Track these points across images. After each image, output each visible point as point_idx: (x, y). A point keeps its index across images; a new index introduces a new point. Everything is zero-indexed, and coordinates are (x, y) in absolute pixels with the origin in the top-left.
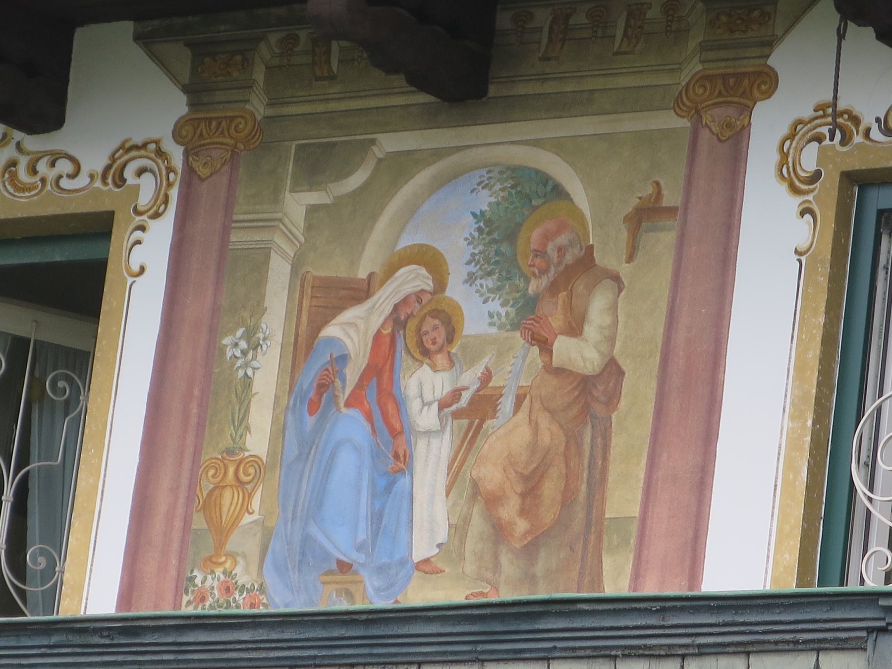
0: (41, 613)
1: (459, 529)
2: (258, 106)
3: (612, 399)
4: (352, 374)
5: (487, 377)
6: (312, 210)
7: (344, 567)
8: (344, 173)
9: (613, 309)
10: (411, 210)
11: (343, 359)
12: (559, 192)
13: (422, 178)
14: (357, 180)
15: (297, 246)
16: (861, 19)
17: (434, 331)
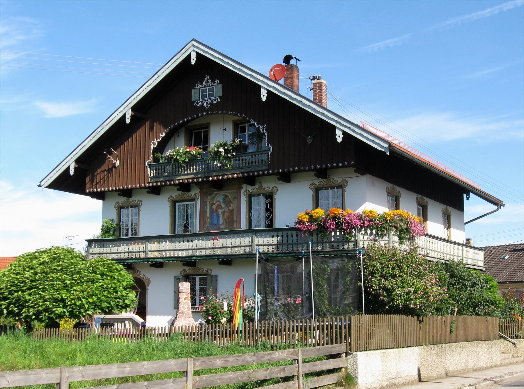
0: (274, 274)
1: (223, 222)
2: (205, 190)
3: (234, 211)
4: (214, 210)
5: (224, 210)
6: (210, 198)
7: (216, 225)
8: (212, 195)
9: (233, 205)
10: (217, 198)
11: (213, 209)
12: (228, 196)
13: (218, 195)
14: (213, 196)
15: (249, 243)
16: (248, 185)
17: (220, 207)
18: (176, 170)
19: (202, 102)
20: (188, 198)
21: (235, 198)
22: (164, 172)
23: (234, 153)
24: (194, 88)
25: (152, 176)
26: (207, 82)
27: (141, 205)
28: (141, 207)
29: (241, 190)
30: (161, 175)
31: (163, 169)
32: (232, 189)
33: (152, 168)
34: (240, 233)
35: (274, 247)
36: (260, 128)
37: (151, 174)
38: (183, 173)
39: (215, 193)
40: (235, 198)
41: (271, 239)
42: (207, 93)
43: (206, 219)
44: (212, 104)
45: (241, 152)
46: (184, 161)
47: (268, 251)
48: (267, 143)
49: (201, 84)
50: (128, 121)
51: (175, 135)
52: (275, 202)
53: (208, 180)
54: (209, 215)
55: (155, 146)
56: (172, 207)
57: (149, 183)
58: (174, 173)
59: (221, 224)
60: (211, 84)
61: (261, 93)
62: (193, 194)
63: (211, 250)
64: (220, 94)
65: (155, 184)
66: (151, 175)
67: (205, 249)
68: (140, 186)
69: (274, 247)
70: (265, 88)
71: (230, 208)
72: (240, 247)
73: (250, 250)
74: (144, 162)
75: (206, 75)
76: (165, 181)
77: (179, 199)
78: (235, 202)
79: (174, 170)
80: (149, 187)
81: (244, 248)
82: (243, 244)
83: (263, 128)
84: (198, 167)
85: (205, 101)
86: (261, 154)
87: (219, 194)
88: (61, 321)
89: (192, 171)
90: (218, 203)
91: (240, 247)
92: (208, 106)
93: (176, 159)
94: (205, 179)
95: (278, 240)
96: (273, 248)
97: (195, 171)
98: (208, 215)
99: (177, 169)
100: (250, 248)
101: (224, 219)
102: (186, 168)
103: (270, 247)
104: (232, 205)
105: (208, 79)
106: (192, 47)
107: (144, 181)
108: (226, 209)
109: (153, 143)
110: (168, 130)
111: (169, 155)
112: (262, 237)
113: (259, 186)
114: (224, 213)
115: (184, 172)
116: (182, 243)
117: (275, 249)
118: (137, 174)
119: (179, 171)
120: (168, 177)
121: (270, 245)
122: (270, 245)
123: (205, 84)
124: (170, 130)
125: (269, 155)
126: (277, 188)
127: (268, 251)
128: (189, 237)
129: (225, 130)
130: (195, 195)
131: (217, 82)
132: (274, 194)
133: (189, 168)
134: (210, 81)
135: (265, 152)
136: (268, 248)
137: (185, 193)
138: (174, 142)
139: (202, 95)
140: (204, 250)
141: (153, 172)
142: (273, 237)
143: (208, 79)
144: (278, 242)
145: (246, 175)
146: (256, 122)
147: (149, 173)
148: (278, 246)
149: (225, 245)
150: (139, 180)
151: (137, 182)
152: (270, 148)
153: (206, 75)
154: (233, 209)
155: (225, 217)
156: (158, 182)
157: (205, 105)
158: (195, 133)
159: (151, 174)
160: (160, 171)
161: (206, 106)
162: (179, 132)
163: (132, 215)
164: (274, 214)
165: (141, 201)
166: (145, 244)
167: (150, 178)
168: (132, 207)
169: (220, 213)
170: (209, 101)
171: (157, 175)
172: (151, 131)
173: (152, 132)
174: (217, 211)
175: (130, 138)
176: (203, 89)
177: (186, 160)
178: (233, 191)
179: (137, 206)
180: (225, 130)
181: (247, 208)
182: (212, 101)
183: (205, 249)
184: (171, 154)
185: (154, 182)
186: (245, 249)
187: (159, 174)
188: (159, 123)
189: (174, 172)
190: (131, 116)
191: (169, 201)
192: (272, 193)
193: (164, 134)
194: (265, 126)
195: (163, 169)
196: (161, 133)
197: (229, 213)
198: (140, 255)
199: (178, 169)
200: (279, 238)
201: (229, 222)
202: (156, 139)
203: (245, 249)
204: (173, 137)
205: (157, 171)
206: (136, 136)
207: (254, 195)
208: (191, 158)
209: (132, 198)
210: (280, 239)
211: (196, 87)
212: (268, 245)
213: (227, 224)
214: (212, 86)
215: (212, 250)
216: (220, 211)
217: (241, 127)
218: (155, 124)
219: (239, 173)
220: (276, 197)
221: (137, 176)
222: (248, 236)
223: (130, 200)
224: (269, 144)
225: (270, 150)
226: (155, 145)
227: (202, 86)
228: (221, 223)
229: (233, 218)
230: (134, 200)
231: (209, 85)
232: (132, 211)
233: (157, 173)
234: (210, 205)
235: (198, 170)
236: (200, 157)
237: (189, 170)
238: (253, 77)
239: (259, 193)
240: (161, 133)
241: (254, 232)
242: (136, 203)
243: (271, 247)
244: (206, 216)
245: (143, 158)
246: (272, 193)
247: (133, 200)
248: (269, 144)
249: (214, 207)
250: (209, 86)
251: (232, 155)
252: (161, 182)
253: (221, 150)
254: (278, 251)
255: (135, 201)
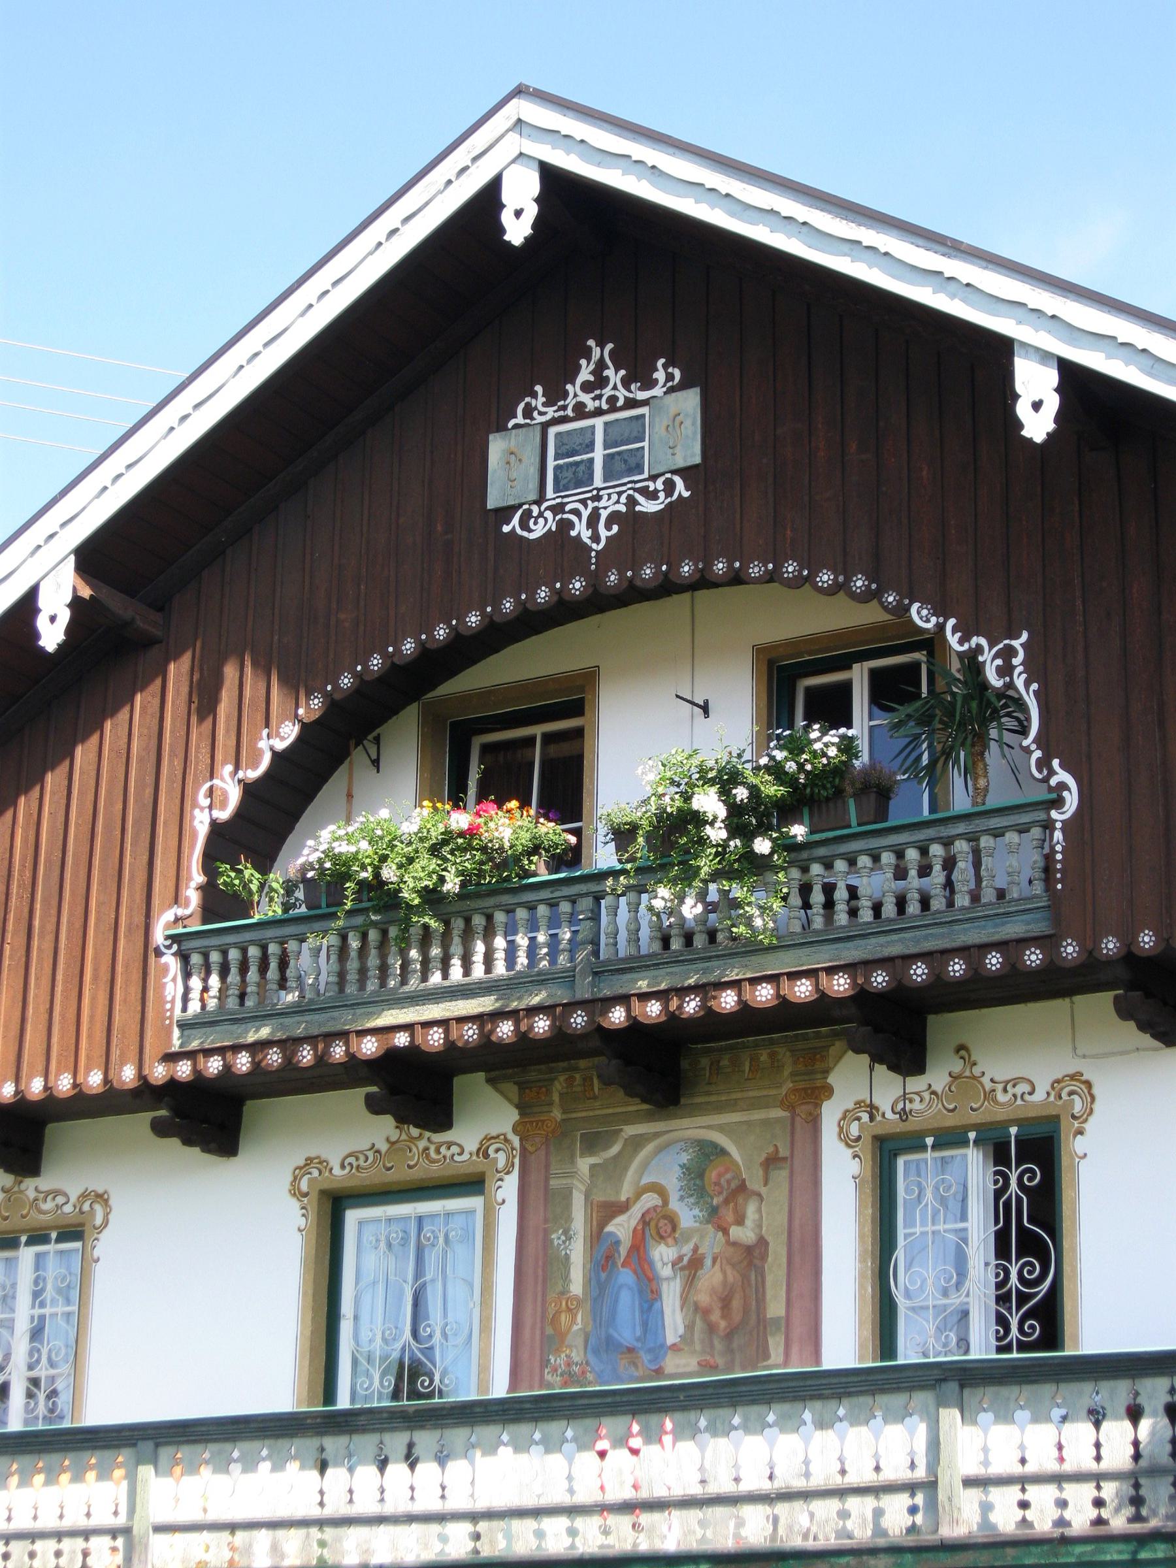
1: (690, 1328)
2: (557, 1114)
3: (764, 1257)
4: (623, 1251)
5: (696, 1249)
6: (593, 1167)
7: (631, 1350)
8: (607, 1147)
9: (759, 1211)
10: (645, 1165)
11: (618, 1243)
12: (723, 1152)
13: (650, 1148)
14: (615, 1149)
18: (363, 972)
19: (558, 509)
20: (434, 1170)
21: (771, 1162)
22: (283, 984)
23: (798, 831)
24: (501, 428)
25: (196, 1016)
26: (600, 381)
27: (106, 1223)
28: (105, 1236)
29: (818, 1106)
30: (261, 1002)
31: (273, 965)
32: (755, 1104)
33: (196, 959)
34: (839, 1397)
35: (1109, 1490)
36: (986, 657)
37: (185, 999)
38: (414, 983)
39: (630, 1130)
40: (771, 1162)
41: (1080, 1433)
42: (598, 455)
43: (558, 1313)
44: (629, 520)
45: (849, 826)
46: (432, 897)
47: (1061, 1522)
48: (1038, 754)
49: (555, 395)
50: (51, 636)
51: (359, 756)
52: (1075, 1184)
53: (600, 1029)
54: (587, 1282)
55: (224, 815)
56: (319, 1235)
57: (171, 1058)
58: (351, 989)
59: (674, 1348)
60: (622, 394)
61: (1019, 388)
62: (471, 1145)
63: (612, 1520)
64: (691, 454)
65: (214, 1065)
66: (184, 1009)
67: (573, 1511)
68: (106, 1081)
69: (1109, 1490)
70: (1045, 356)
71: (735, 1232)
72: (841, 1493)
73: (919, 1519)
74: (140, 919)
75: (591, 343)
76: (289, 1045)
77: (373, 1176)
78: (778, 1191)
79: (353, 965)
80: (172, 1085)
81: (869, 1502)
82: (861, 1474)
83: (1009, 652)
84: (522, 941)
85: (584, 502)
86: (998, 833)
87: (657, 1135)
88: (422, 807)
89: (478, 971)
90: (650, 1200)
91: (841, 1493)
92: (604, 533)
93: (378, 883)
94: (578, 1020)
95: (1136, 1443)
96: (1099, 1503)
97: (500, 969)
98: (576, 1286)
99: (373, 961)
100: (919, 1499)
101: (697, 1307)
102: (435, 951)
103: (1080, 1496)
104: (751, 1210)
105: (601, 365)
106: (513, 137)
107: (134, 1048)
108: (711, 1243)
109: (211, 792)
110: (316, 703)
111: (320, 861)
112: (1013, 1421)
113: (954, 1077)
114: (691, 1267)
115: (424, 979)
116: (397, 1470)
117: (1117, 1510)
118: (93, 999)
119: (384, 969)
120: (309, 1017)
121: (1079, 1477)
122: (1079, 1477)
123: (585, 398)
124: (333, 707)
125: (1058, 835)
126: (1088, 1084)
127: (1061, 1522)
128: (456, 1425)
129: (705, 709)
130: (483, 1152)
131: (670, 377)
132: (1067, 1126)
133: (456, 948)
134: (614, 376)
135: (1025, 818)
136: (1062, 1504)
137: (412, 1139)
138: (350, 796)
139: (557, 468)
140: (562, 1522)
141: (205, 989)
142: (1097, 1417)
143: (601, 365)
144: (1137, 1457)
145: (880, 979)
146: (952, 622)
147: (173, 988)
148: (1137, 1486)
149: (722, 1485)
150: (100, 1035)
151: (88, 1057)
152: (1063, 786)
153: (591, 343)
154: (762, 1242)
155: (703, 1298)
156: (236, 1048)
157: (581, 530)
158: (486, 749)
159: (185, 999)
160: (253, 975)
161: (586, 535)
162: (377, 740)
163: (36, 1295)
164: (1067, 1268)
165: (102, 1198)
166: (126, 1477)
167: (183, 1026)
168: (39, 1238)
169: (666, 1272)
170: (610, 505)
171: (232, 1003)
172: (201, 719)
173: (208, 723)
174: (639, 1248)
175: (53, 768)
176: (568, 433)
177: (446, 887)
178: (757, 1115)
179: (73, 1232)
180: (705, 709)
181: (868, 1228)
182: (632, 502)
183: (573, 1511)
184: (343, 848)
185: (208, 1053)
186: (878, 1513)
187: (242, 996)
188: (255, 664)
189: (352, 976)
190: (71, 606)
191: (296, 1193)
192: (1055, 1120)
193: (287, 734)
194: (1016, 643)
195: (273, 965)
196: (267, 726)
197: (733, 1266)
198: (86, 1554)
199: (383, 957)
200: (1145, 1424)
201: (729, 1336)
202: (229, 768)
203: (878, 1513)
204: (343, 770)
205: (233, 977)
206: (93, 756)
207: (912, 1142)
208: (481, 874)
209: (45, 1182)
210: (1153, 1433)
211: (520, 419)
212: (1058, 1479)
213: (718, 1345)
214: (631, 404)
215: (621, 1523)
216: (662, 1255)
217: (809, 691)
218: (230, 672)
219: (831, 971)
220: (1080, 1145)
221: (92, 1017)
222: (899, 1416)
223: (31, 1194)
224: (1056, 763)
225: (1058, 803)
226: (223, 805)
227: (564, 408)
228: (671, 1338)
229: (761, 1301)
230: (57, 1193)
231: (612, 400)
232: (37, 1267)
233: (234, 991)
234: (588, 1220)
235: (522, 960)
236: (542, 869)
237: (456, 963)
238: (952, 286)
239: (951, 1121)
240: (267, 726)
241: (953, 1386)
242: (68, 1209)
243: (1087, 1491)
244: (565, 1292)
245: (140, 897)
246: (1055, 1120)
247: (48, 1193)
248: (1056, 763)
249: (622, 1227)
250: (613, 409)
251: (789, 846)
252: (257, 1048)
253: (709, 802)
254: (1137, 1518)
255: (60, 1200)
